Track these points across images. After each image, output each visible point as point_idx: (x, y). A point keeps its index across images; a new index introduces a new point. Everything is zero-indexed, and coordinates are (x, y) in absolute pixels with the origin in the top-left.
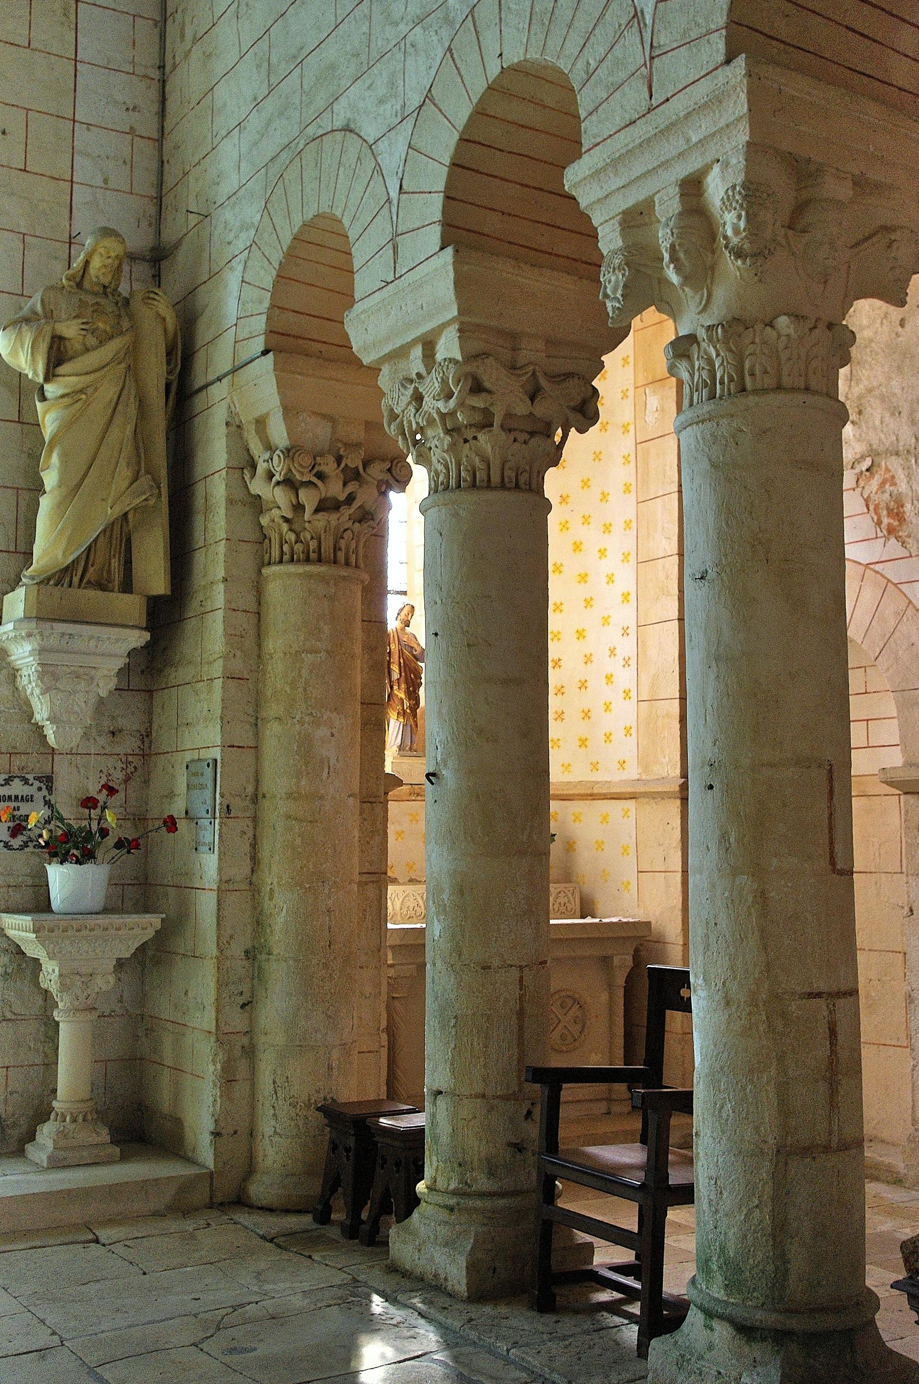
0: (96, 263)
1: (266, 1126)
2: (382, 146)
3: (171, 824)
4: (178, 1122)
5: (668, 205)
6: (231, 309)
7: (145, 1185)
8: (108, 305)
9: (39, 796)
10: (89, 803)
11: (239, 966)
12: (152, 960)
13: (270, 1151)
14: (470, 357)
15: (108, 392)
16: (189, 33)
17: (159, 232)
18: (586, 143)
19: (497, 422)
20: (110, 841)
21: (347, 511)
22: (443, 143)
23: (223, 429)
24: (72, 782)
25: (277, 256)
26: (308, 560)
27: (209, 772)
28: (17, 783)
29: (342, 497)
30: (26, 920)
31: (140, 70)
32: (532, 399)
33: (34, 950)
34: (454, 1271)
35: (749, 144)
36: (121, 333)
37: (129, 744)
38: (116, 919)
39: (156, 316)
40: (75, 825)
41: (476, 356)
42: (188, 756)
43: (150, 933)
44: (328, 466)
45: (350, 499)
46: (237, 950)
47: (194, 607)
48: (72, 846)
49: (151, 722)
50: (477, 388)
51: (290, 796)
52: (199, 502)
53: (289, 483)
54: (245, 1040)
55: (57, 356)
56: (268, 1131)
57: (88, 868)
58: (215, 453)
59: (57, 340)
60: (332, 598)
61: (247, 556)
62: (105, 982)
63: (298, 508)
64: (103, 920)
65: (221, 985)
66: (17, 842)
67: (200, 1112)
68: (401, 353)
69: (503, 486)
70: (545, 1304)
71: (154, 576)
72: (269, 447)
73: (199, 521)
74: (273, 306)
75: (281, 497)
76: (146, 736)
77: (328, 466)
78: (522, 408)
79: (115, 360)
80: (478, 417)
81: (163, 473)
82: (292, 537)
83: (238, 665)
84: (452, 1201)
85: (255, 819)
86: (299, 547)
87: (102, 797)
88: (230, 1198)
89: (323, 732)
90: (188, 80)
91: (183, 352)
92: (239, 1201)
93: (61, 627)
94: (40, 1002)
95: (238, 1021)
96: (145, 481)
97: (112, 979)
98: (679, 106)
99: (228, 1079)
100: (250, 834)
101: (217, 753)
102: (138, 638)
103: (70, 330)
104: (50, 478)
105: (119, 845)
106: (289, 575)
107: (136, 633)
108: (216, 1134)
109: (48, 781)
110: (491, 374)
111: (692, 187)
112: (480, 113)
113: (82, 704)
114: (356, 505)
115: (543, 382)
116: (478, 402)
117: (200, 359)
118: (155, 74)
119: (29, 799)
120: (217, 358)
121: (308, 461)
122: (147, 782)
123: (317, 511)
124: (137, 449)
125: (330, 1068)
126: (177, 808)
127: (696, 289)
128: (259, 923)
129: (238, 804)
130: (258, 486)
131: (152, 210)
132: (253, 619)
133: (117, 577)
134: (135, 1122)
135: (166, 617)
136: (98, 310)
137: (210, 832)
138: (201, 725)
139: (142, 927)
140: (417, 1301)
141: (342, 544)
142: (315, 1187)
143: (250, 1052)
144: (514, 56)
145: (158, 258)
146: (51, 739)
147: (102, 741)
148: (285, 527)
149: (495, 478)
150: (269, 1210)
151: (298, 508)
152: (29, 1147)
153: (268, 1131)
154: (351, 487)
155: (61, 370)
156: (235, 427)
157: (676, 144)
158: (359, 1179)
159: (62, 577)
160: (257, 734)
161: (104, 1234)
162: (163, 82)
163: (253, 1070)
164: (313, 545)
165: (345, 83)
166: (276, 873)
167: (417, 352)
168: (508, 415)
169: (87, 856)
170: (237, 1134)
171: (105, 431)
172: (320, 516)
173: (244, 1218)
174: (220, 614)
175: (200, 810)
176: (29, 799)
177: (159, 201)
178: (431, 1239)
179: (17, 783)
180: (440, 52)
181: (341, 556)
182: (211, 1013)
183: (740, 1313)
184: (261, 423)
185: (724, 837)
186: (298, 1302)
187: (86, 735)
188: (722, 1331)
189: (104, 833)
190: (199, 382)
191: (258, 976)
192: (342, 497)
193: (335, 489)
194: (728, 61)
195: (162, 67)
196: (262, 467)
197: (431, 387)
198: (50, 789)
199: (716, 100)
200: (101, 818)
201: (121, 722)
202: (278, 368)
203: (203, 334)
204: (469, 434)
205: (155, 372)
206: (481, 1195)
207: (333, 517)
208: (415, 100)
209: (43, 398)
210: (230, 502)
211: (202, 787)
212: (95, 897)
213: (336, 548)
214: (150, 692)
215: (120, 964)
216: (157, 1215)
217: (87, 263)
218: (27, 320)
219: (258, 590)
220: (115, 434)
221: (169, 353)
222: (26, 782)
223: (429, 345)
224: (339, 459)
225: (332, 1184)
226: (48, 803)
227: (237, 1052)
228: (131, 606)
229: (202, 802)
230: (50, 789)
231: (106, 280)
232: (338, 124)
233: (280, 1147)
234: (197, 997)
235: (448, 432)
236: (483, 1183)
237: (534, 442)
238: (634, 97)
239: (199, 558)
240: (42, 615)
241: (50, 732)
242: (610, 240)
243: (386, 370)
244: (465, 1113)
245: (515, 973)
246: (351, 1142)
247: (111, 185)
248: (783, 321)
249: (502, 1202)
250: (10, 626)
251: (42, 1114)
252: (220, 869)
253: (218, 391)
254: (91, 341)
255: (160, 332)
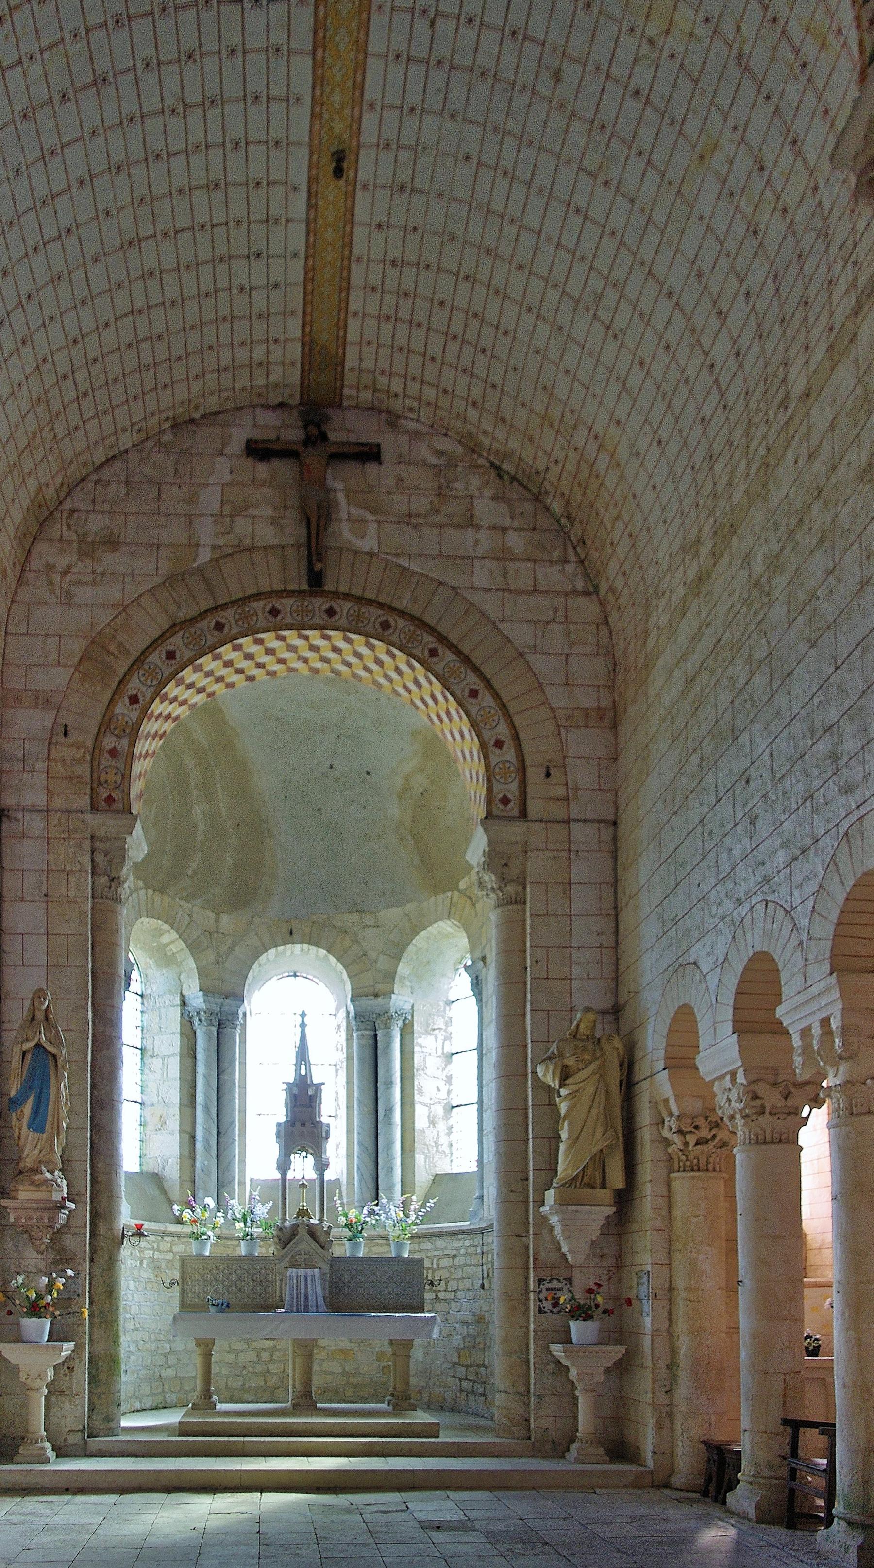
0: (582, 1026)
1: (679, 1450)
2: (708, 977)
3: (629, 1302)
4: (638, 1448)
5: (816, 1031)
6: (650, 1043)
7: (618, 1473)
8: (590, 1046)
9: (565, 1288)
10: (590, 1291)
11: (663, 1373)
12: (623, 1368)
13: (681, 1464)
14: (750, 1083)
15: (590, 1090)
16: (628, 892)
17: (617, 995)
18: (784, 998)
19: (767, 1111)
20: (601, 1309)
21: (712, 1144)
22: (732, 982)
23: (648, 1105)
24: (581, 1281)
25: (668, 1021)
26: (692, 1170)
27: (646, 1277)
28: (555, 1282)
29: (709, 1137)
30: (559, 1347)
31: (603, 912)
32: (786, 1098)
33: (565, 1362)
34: (751, 1512)
35: (843, 1009)
36: (596, 1059)
37: (609, 1262)
38: (603, 1348)
39: (614, 1050)
40: (582, 1302)
41: (754, 1082)
42: (637, 1268)
43: (620, 1355)
44: (700, 1122)
45: (714, 1137)
46: (662, 1364)
47: (637, 1194)
48: (582, 1312)
49: (621, 1250)
50: (756, 1097)
51: (685, 1289)
52: (638, 1141)
53: (680, 1132)
54: (668, 1409)
55: (565, 1075)
56: (680, 1453)
57: (589, 1323)
58: (645, 1117)
59: (565, 1067)
60: (706, 1189)
61: (662, 1170)
62: (599, 1377)
63: (686, 1144)
64: (595, 1348)
65: (655, 1380)
66: (556, 1310)
67: (648, 1440)
68: (722, 1077)
69: (772, 1142)
70: (791, 1525)
71: (617, 1180)
72: (671, 1115)
73: (639, 1151)
74: (667, 1045)
75: (676, 1138)
76: (619, 1257)
77: (700, 1122)
78: (780, 1103)
79: (594, 1073)
80: (758, 1110)
81: (619, 1128)
82: (684, 1158)
83: (658, 1224)
84: (751, 1479)
85: (670, 1300)
86: (688, 1163)
87: (595, 1288)
88: (661, 1483)
89: (702, 1257)
90: (626, 916)
91: (628, 1065)
92: (667, 1486)
93: (570, 1208)
94: (570, 1387)
95: (663, 1399)
96: (610, 1133)
97: (602, 1376)
98: (814, 990)
99: (659, 1427)
100: (667, 1307)
101: (649, 1268)
102: (610, 1211)
103: (570, 1061)
104: (564, 1135)
105: (605, 1312)
106: (683, 1178)
107: (609, 1208)
108: (654, 1453)
109: (570, 1280)
110: (762, 1089)
111: (825, 1022)
112: (746, 969)
113: (584, 1246)
114: (717, 1140)
115: (793, 1090)
116: (758, 1103)
117: (637, 1068)
118: (612, 912)
119: (560, 1289)
120: (642, 1070)
121: (689, 1121)
122: (620, 1280)
123: (696, 1144)
124: (606, 1118)
125: (710, 1424)
126: (632, 1295)
127: (832, 1066)
128: (673, 1352)
129: (660, 1294)
130: (666, 1133)
131: (613, 985)
132: (667, 1200)
133: (598, 1181)
134: (620, 1449)
135: (625, 1200)
136: (584, 1049)
137: (647, 1306)
138: (646, 1253)
139: (617, 1351)
140: (732, 1521)
141: (711, 1160)
142: (701, 1481)
143: (670, 1415)
144: (758, 949)
145: (616, 1011)
146: (570, 1260)
147: (596, 1260)
148: (680, 1153)
149: (768, 1138)
150: (677, 1489)
151: (686, 1144)
152: (567, 1455)
153: (680, 1453)
154: (713, 1132)
155: (567, 1082)
156: (654, 1103)
157: (814, 1006)
158: (718, 1473)
159: (572, 1182)
160: (670, 1258)
161: (598, 1491)
162: (617, 916)
163: (672, 1423)
164: (695, 1161)
165: (694, 941)
166: (681, 1326)
167: (728, 1077)
168: (773, 1107)
169: (588, 1317)
170: (665, 1453)
171: (589, 1111)
172: (698, 1147)
173: (666, 1492)
174: (649, 1198)
175: (643, 1295)
176: (560, 1289)
177: (616, 979)
178: (743, 1498)
179: (555, 1282)
180: (730, 937)
181: (710, 1167)
182: (650, 1395)
183: (848, 1516)
184: (666, 1101)
185: (843, 1313)
186: (678, 1517)
187: (587, 1258)
188: (843, 1524)
189: (597, 1306)
190: (636, 1079)
191: (674, 1378)
192: (709, 1137)
193: (705, 1133)
194: (831, 974)
195: (616, 908)
196: (666, 1123)
197: (734, 1096)
198: (571, 1284)
199: (827, 990)
200: (595, 1299)
201: (605, 1251)
202: (670, 1078)
203: (638, 1055)
204: (754, 1118)
205: (614, 1075)
206: (765, 1477)
207: (705, 1147)
208: (721, 959)
209: (560, 1096)
210: (652, 1141)
211: (643, 1284)
212: (591, 1337)
213: (708, 1163)
214: (620, 1235)
215: (607, 1371)
216: (625, 1486)
217: (578, 1026)
218: (550, 1058)
219: (669, 1184)
220: (594, 1111)
221: (621, 1065)
222: (559, 1281)
223: (733, 1074)
224: (706, 1118)
225: (709, 1480)
226: (570, 1291)
227: (664, 1414)
228: (605, 1195)
229: (643, 1291)
230: (571, 1284)
231: (588, 1033)
232: (692, 961)
233: (687, 1462)
234: (645, 1387)
235: (743, 1117)
236: (766, 1473)
237: (789, 1118)
238: (799, 981)
239: (639, 1169)
240: (562, 1203)
241: (569, 1257)
242: (796, 1041)
243: (716, 1083)
244: (756, 1440)
245: (782, 1376)
246: (716, 1457)
247: (592, 976)
248: (869, 1081)
249: (775, 1481)
250: (548, 1208)
251: (572, 1440)
252: (652, 1325)
253: (645, 1085)
254: (581, 1066)
255: (616, 1055)
